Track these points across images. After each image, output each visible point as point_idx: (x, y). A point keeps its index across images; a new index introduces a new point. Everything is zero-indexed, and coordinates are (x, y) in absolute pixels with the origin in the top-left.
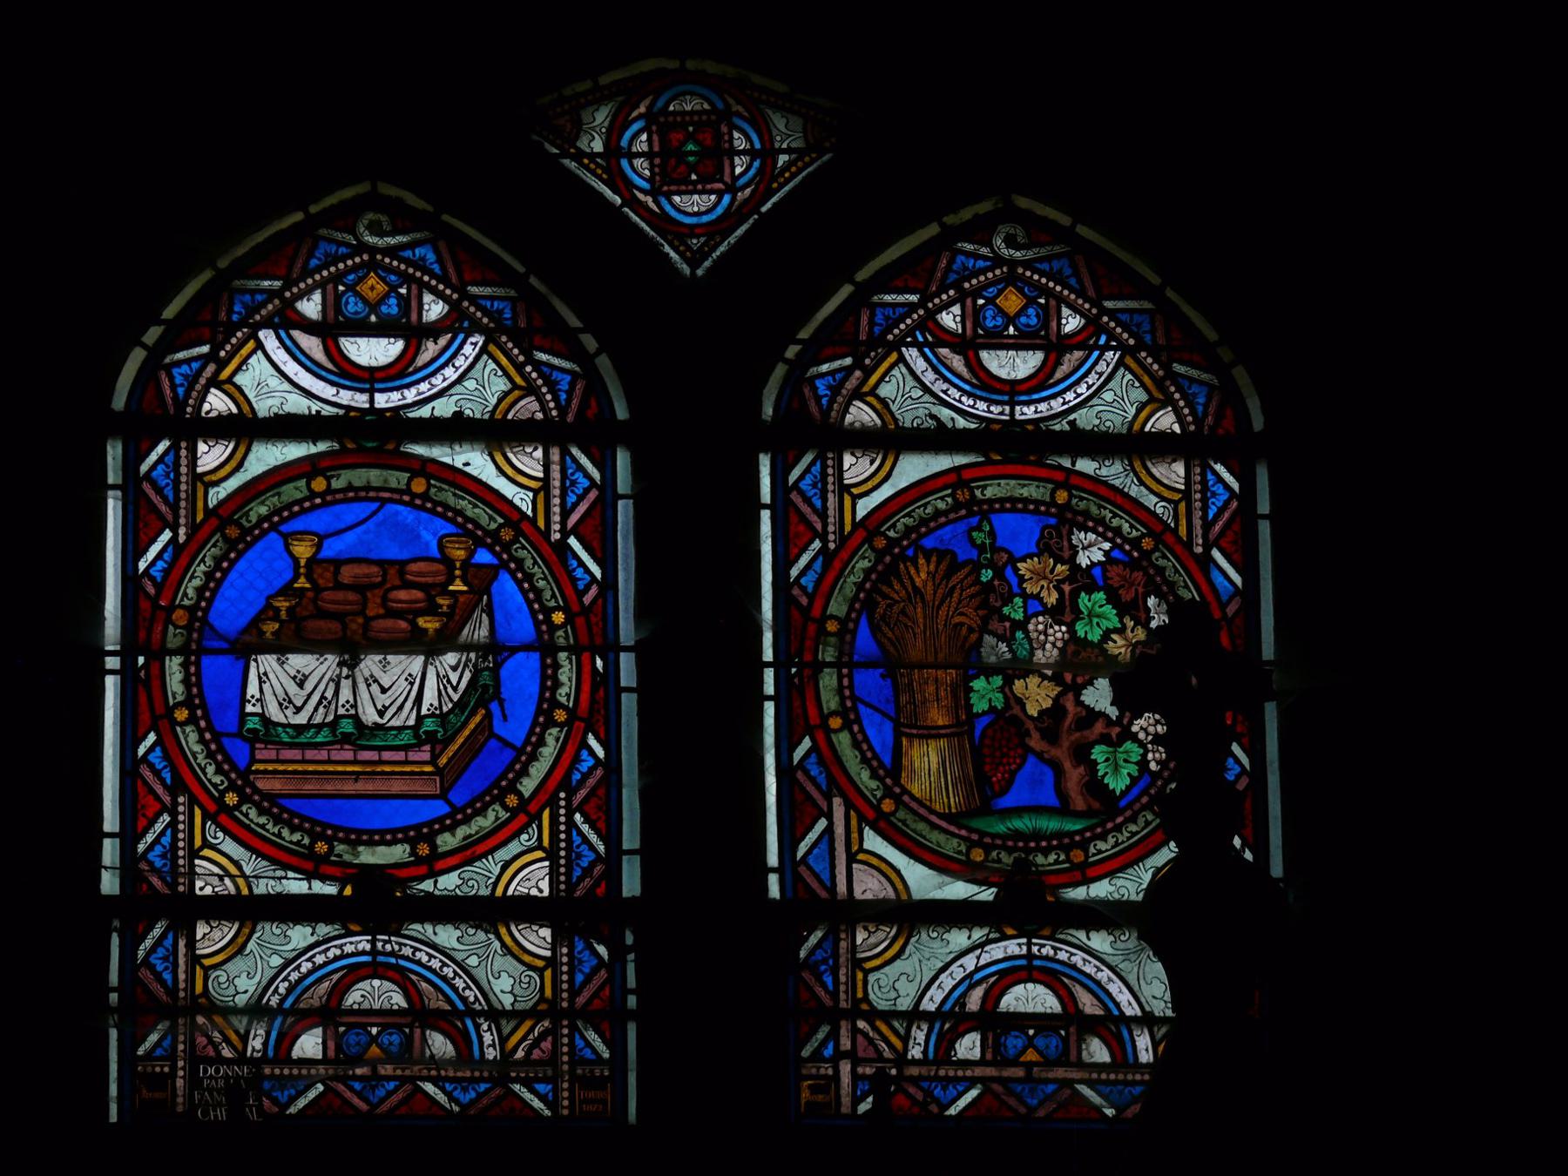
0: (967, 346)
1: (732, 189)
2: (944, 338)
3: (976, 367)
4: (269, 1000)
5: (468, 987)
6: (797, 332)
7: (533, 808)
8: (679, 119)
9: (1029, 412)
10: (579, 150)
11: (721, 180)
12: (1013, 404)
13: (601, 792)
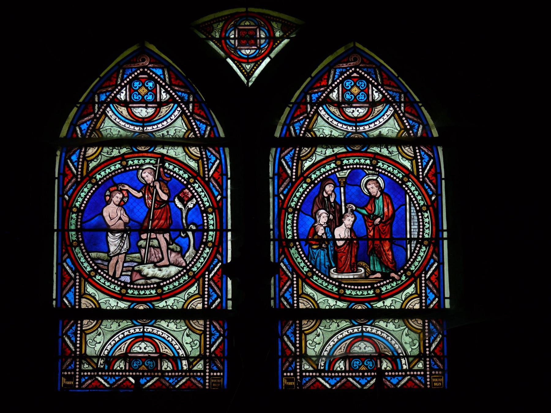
0: (338, 105)
1: (259, 48)
2: (333, 103)
3: (131, 114)
4: (405, 359)
5: (110, 344)
6: (291, 100)
7: (197, 277)
8: (204, 25)
9: (149, 129)
10: (212, 36)
11: (238, 46)
12: (143, 127)
13: (436, 273)
